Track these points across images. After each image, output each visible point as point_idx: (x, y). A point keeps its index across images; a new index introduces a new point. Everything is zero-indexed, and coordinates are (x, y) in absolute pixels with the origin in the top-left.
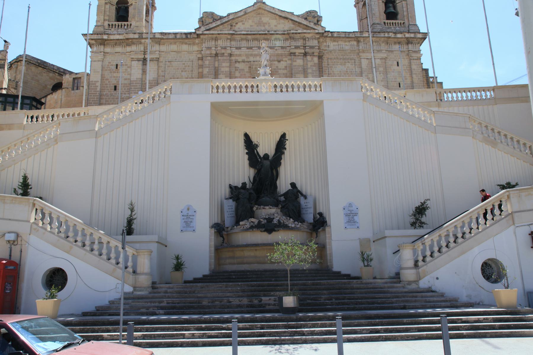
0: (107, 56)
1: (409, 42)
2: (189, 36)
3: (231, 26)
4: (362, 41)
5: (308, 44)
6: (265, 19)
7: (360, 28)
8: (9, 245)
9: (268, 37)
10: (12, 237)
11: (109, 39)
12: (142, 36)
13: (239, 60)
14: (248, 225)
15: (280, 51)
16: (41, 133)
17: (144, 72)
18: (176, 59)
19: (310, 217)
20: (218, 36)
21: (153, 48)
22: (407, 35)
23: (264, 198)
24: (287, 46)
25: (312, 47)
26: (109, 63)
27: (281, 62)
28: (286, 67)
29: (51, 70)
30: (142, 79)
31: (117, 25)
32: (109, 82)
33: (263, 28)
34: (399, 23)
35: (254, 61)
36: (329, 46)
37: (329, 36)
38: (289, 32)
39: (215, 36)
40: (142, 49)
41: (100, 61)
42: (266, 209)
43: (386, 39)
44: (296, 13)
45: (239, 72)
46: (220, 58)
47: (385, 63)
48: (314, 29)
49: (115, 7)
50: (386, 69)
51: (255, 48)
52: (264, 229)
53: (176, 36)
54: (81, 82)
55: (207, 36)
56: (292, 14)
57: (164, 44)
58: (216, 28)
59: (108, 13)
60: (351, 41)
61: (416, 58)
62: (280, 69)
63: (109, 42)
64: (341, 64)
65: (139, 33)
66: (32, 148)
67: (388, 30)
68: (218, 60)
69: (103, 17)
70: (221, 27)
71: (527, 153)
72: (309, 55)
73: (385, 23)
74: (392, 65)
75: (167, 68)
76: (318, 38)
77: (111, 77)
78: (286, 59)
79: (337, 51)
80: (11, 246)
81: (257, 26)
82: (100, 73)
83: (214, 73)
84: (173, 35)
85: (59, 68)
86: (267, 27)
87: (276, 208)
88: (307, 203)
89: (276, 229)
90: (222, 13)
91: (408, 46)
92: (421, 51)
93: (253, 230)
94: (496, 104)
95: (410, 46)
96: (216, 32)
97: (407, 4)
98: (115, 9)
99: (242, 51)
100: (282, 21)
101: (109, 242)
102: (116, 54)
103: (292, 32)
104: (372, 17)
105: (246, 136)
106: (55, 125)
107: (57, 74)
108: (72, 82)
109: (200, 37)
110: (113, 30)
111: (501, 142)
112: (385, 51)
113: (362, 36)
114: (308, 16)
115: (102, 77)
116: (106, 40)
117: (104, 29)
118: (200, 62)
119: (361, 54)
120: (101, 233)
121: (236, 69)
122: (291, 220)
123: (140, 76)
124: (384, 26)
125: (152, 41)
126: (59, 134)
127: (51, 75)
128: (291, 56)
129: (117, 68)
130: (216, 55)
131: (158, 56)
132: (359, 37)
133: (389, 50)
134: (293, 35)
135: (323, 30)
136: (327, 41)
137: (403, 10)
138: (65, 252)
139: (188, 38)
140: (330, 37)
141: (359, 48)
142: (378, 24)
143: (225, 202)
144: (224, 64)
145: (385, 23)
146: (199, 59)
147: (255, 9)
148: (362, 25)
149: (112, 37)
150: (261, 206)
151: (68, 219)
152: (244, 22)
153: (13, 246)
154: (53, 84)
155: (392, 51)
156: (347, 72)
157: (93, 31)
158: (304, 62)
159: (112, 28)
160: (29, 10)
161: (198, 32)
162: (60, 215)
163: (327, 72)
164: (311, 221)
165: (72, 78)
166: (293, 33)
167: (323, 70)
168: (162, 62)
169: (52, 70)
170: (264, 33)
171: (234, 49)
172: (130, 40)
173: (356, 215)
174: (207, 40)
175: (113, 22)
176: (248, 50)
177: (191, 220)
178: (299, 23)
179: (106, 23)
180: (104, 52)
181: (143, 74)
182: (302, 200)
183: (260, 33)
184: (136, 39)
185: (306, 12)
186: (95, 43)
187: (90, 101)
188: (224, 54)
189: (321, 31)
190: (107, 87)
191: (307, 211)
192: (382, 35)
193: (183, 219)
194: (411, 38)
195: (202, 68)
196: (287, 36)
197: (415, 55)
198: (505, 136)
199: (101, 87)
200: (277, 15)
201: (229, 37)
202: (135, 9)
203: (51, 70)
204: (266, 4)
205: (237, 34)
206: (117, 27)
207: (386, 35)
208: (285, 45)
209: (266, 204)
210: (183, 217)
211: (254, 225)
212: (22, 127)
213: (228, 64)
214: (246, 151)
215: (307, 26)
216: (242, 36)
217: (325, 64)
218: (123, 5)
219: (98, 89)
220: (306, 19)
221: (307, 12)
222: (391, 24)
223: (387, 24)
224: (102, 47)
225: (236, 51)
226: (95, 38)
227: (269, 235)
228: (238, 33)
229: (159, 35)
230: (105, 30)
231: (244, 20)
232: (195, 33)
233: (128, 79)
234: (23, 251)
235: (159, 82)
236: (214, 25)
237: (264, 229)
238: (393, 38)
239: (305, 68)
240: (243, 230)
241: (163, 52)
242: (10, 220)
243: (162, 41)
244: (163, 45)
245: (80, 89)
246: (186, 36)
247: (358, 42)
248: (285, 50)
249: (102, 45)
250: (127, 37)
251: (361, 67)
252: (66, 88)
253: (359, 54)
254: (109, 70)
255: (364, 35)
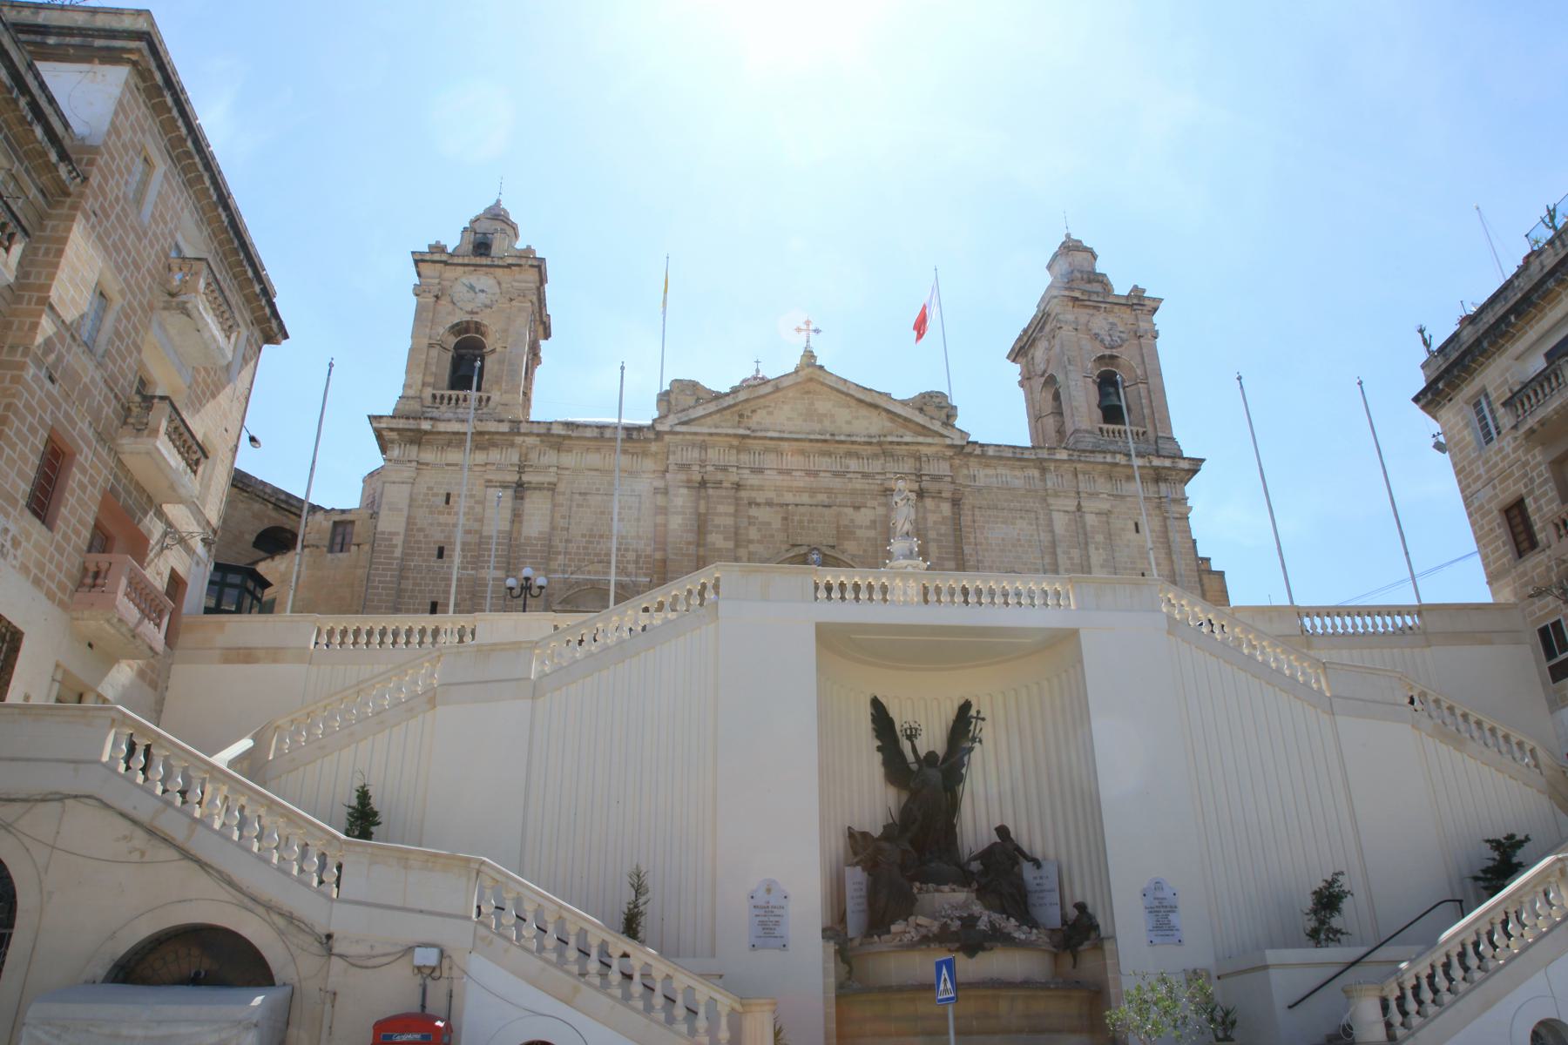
0: (424, 472)
1: (1158, 476)
2: (635, 435)
3: (741, 416)
4: (1052, 468)
5: (929, 469)
6: (823, 406)
7: (1038, 435)
8: (418, 980)
9: (831, 447)
10: (428, 957)
11: (435, 430)
12: (518, 429)
13: (758, 500)
14: (913, 934)
15: (859, 484)
16: (390, 679)
17: (517, 516)
18: (598, 489)
19: (1051, 916)
20: (707, 438)
21: (542, 458)
22: (1156, 462)
23: (933, 865)
24: (878, 473)
25: (936, 478)
26: (430, 488)
27: (863, 510)
28: (874, 522)
29: (258, 496)
30: (511, 532)
31: (454, 397)
32: (426, 536)
33: (817, 427)
34: (1135, 431)
35: (797, 505)
36: (975, 476)
37: (976, 452)
38: (882, 439)
39: (701, 438)
40: (515, 459)
41: (407, 483)
42: (942, 892)
43: (1107, 467)
44: (897, 396)
45: (759, 530)
46: (711, 491)
47: (1108, 523)
48: (942, 436)
49: (450, 354)
50: (1111, 540)
51: (799, 473)
52: (957, 945)
53: (602, 433)
54: (352, 534)
55: (680, 437)
56: (888, 395)
57: (570, 450)
58: (703, 420)
59: (434, 369)
60: (1026, 467)
61: (1178, 516)
62: (861, 527)
63: (431, 437)
64: (1004, 522)
65: (511, 421)
66: (368, 717)
67: (1111, 448)
68: (708, 497)
69: (420, 376)
70: (717, 417)
71: (1527, 765)
72: (928, 497)
73: (1101, 429)
74: (1123, 529)
75: (574, 509)
76: (951, 458)
77: (431, 524)
78: (875, 503)
79: (995, 490)
80: (425, 979)
81: (805, 420)
82: (405, 513)
83: (696, 528)
84: (596, 430)
85: (277, 491)
86: (827, 423)
87: (966, 889)
88: (1041, 878)
89: (986, 945)
90: (720, 382)
91: (1159, 487)
92: (1187, 499)
93: (929, 946)
94: (1429, 646)
95: (1163, 486)
96: (705, 430)
97: (1149, 392)
98: (450, 359)
99: (766, 477)
100: (864, 412)
101: (668, 977)
102: (446, 468)
103: (889, 439)
104: (1073, 415)
105: (877, 704)
106: (428, 661)
107: (270, 506)
108: (330, 530)
109: (662, 440)
110: (444, 408)
111: (1472, 737)
112: (1105, 496)
113: (1053, 457)
114: (925, 404)
115: (408, 523)
116: (426, 432)
117: (423, 406)
118: (660, 500)
119: (1051, 500)
120: (649, 954)
121: (752, 521)
122: (1012, 920)
123: (505, 526)
124: (1100, 437)
125: (542, 441)
126: (440, 685)
127: (257, 506)
128: (886, 496)
129: (447, 502)
130: (703, 484)
131: (554, 480)
132: (1045, 460)
133: (1115, 493)
134: (890, 447)
135: (962, 438)
136: (971, 464)
137: (1141, 403)
138: (561, 1000)
139: (632, 438)
140: (977, 456)
141: (1046, 485)
142: (1087, 431)
143: (848, 870)
144: (721, 509)
145: (1101, 429)
146: (656, 491)
147: (799, 380)
148: (1040, 431)
149: (442, 427)
150: (930, 885)
151: (565, 915)
152: (771, 409)
153: (429, 982)
154: (259, 531)
155: (1122, 497)
156: (1019, 540)
157: (395, 410)
158: (917, 512)
159: (441, 403)
160: (330, 370)
161: (659, 428)
162: (545, 903)
163: (972, 540)
164: (1056, 922)
165: (331, 522)
166: (891, 443)
167: (963, 534)
168: (564, 494)
169: (262, 494)
170: (823, 437)
171: (747, 471)
172: (487, 437)
173: (1174, 912)
174: (680, 448)
175: (443, 389)
176: (781, 477)
177: (777, 919)
178: (906, 419)
179: (428, 392)
180: (418, 462)
181: (513, 522)
182: (1028, 871)
183: (812, 437)
184: (503, 434)
185: (920, 394)
186: (397, 437)
187: (374, 581)
188: (721, 482)
189: (958, 442)
190: (419, 549)
191: (1042, 898)
192: (1099, 458)
193: (757, 916)
194: (1164, 468)
195: (666, 514)
196: (877, 449)
197: (1175, 509)
198: (1479, 724)
199: (404, 548)
200: (852, 396)
201: (735, 442)
202: (501, 362)
203: (258, 496)
204: (825, 371)
205: (755, 438)
206: (453, 401)
207: (1109, 459)
208: (870, 470)
209: (940, 880)
210: (757, 912)
211: (931, 935)
212: (302, 656)
213: (731, 509)
214: (878, 743)
215: (924, 427)
216: (767, 442)
217: (966, 519)
218: (471, 351)
219: (398, 553)
220: (921, 410)
221: (923, 396)
222: (1117, 434)
223: (1108, 432)
224: (415, 448)
225: (777, 477)
226: (401, 426)
227: (970, 960)
228: (759, 434)
229: (561, 427)
230: (425, 409)
231: (773, 405)
232: (650, 428)
233: (476, 532)
234: (454, 994)
235: (553, 543)
236: (700, 411)
237: (957, 945)
238: (1124, 466)
239: (920, 526)
240: (901, 946)
241: (567, 469)
242: (421, 911)
243: (566, 442)
244: (567, 451)
245: (349, 550)
246: (628, 435)
247: (1044, 470)
248: (870, 481)
249: (415, 443)
250: (479, 429)
251: (1052, 531)
252: (313, 546)
253: (1045, 500)
254: (427, 507)
255: (1058, 457)
